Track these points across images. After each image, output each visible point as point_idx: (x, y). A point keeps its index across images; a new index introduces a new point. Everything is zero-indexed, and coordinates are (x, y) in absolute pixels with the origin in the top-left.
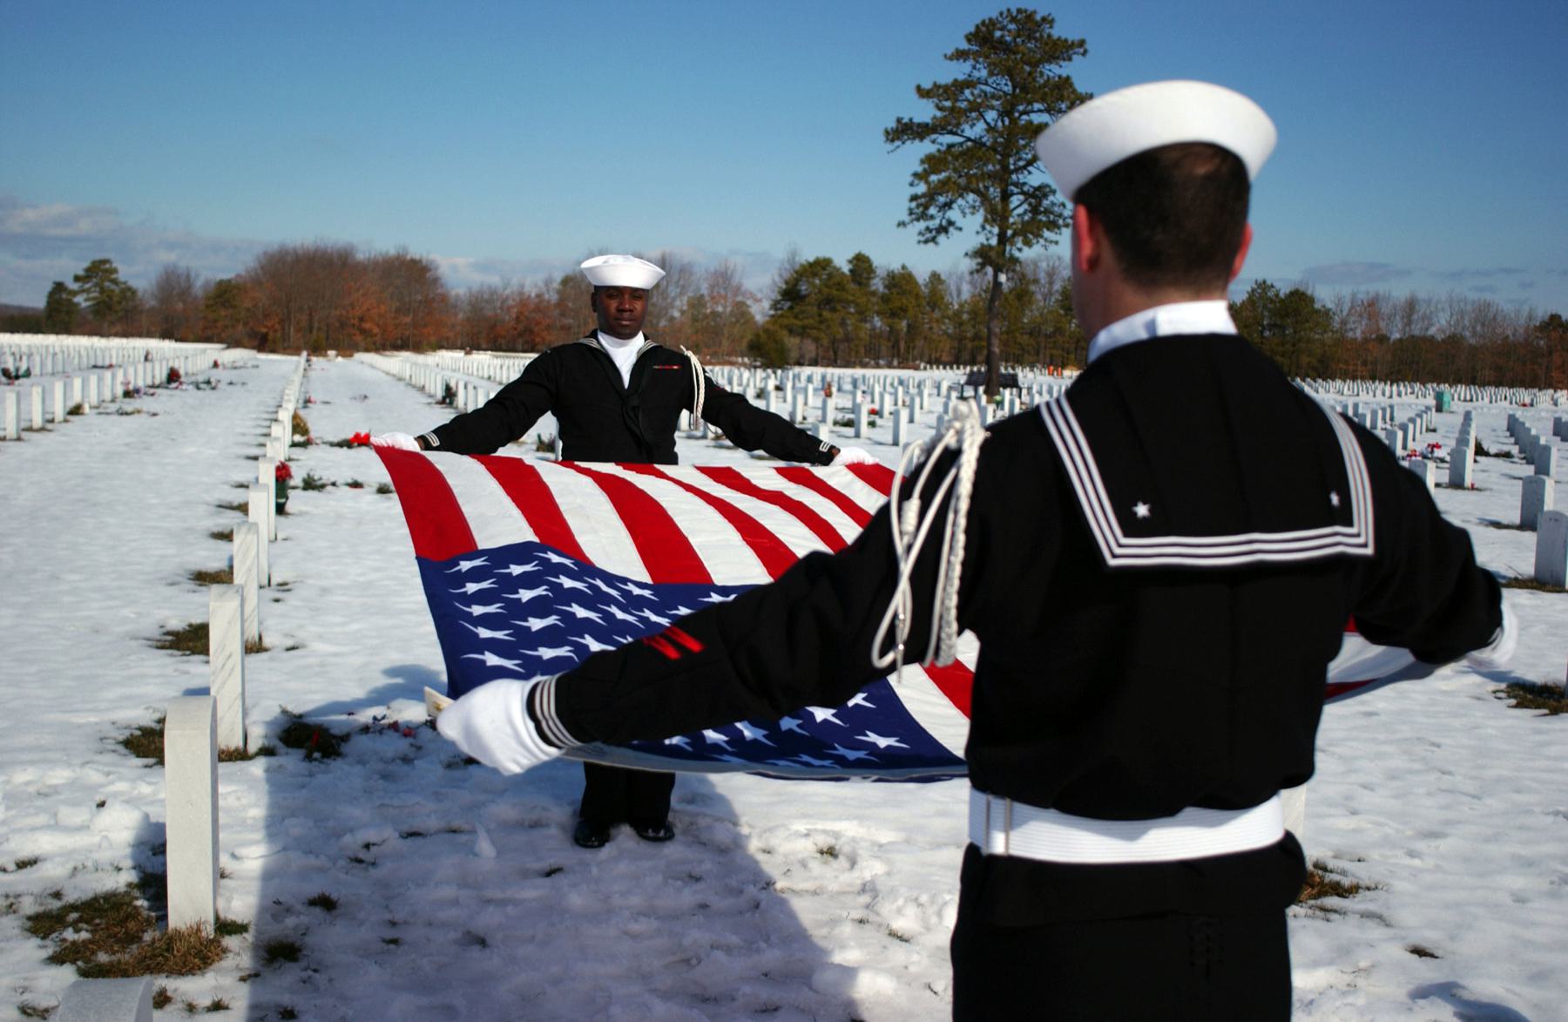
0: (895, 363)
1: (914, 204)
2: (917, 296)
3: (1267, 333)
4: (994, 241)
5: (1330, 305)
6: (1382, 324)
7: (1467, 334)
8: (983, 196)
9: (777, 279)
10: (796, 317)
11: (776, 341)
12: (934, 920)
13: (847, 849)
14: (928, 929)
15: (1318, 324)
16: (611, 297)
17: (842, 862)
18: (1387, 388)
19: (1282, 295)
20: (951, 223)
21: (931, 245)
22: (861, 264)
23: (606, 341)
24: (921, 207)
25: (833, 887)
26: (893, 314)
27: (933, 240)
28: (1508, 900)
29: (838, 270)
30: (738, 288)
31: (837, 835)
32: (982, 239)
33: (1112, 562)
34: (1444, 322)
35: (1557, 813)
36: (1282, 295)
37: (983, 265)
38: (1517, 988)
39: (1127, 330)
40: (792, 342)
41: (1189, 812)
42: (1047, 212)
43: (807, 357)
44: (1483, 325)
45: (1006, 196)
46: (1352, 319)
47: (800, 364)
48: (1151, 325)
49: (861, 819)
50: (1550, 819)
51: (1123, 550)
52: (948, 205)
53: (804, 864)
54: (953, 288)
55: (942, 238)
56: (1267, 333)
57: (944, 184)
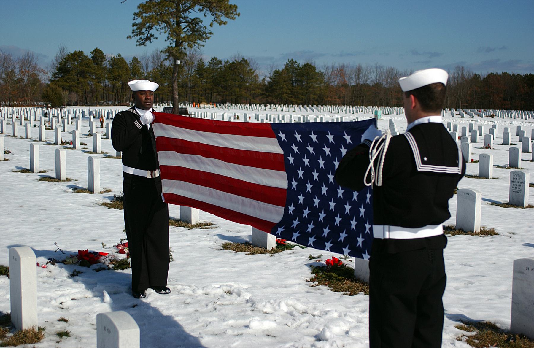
0: (117, 103)
1: (135, 28)
2: (127, 70)
3: (294, 84)
4: (174, 45)
5: (323, 71)
6: (346, 79)
7: (384, 83)
8: (168, 23)
9: (55, 62)
10: (66, 81)
11: (56, 94)
12: (277, 307)
13: (236, 290)
14: (275, 311)
15: (318, 80)
16: (142, 94)
17: (234, 296)
18: (351, 109)
19: (301, 66)
20: (152, 36)
21: (143, 46)
22: (98, 54)
23: (139, 112)
24: (139, 29)
25: (236, 302)
26: (115, 79)
27: (144, 43)
28: (454, 289)
29: (86, 57)
30: (35, 67)
31: (231, 286)
32: (167, 44)
33: (419, 170)
34: (373, 78)
35: (462, 265)
36: (301, 66)
37: (169, 56)
38: (462, 309)
39: (425, 120)
40: (65, 94)
41: (428, 226)
42: (197, 31)
43: (72, 102)
44: (391, 79)
45: (178, 23)
46: (333, 77)
47: (69, 105)
48: (429, 120)
49: (235, 281)
50: (460, 266)
51: (421, 167)
52: (151, 27)
53: (222, 296)
54: (144, 64)
55: (148, 43)
56: (294, 84)
57: (151, 18)
